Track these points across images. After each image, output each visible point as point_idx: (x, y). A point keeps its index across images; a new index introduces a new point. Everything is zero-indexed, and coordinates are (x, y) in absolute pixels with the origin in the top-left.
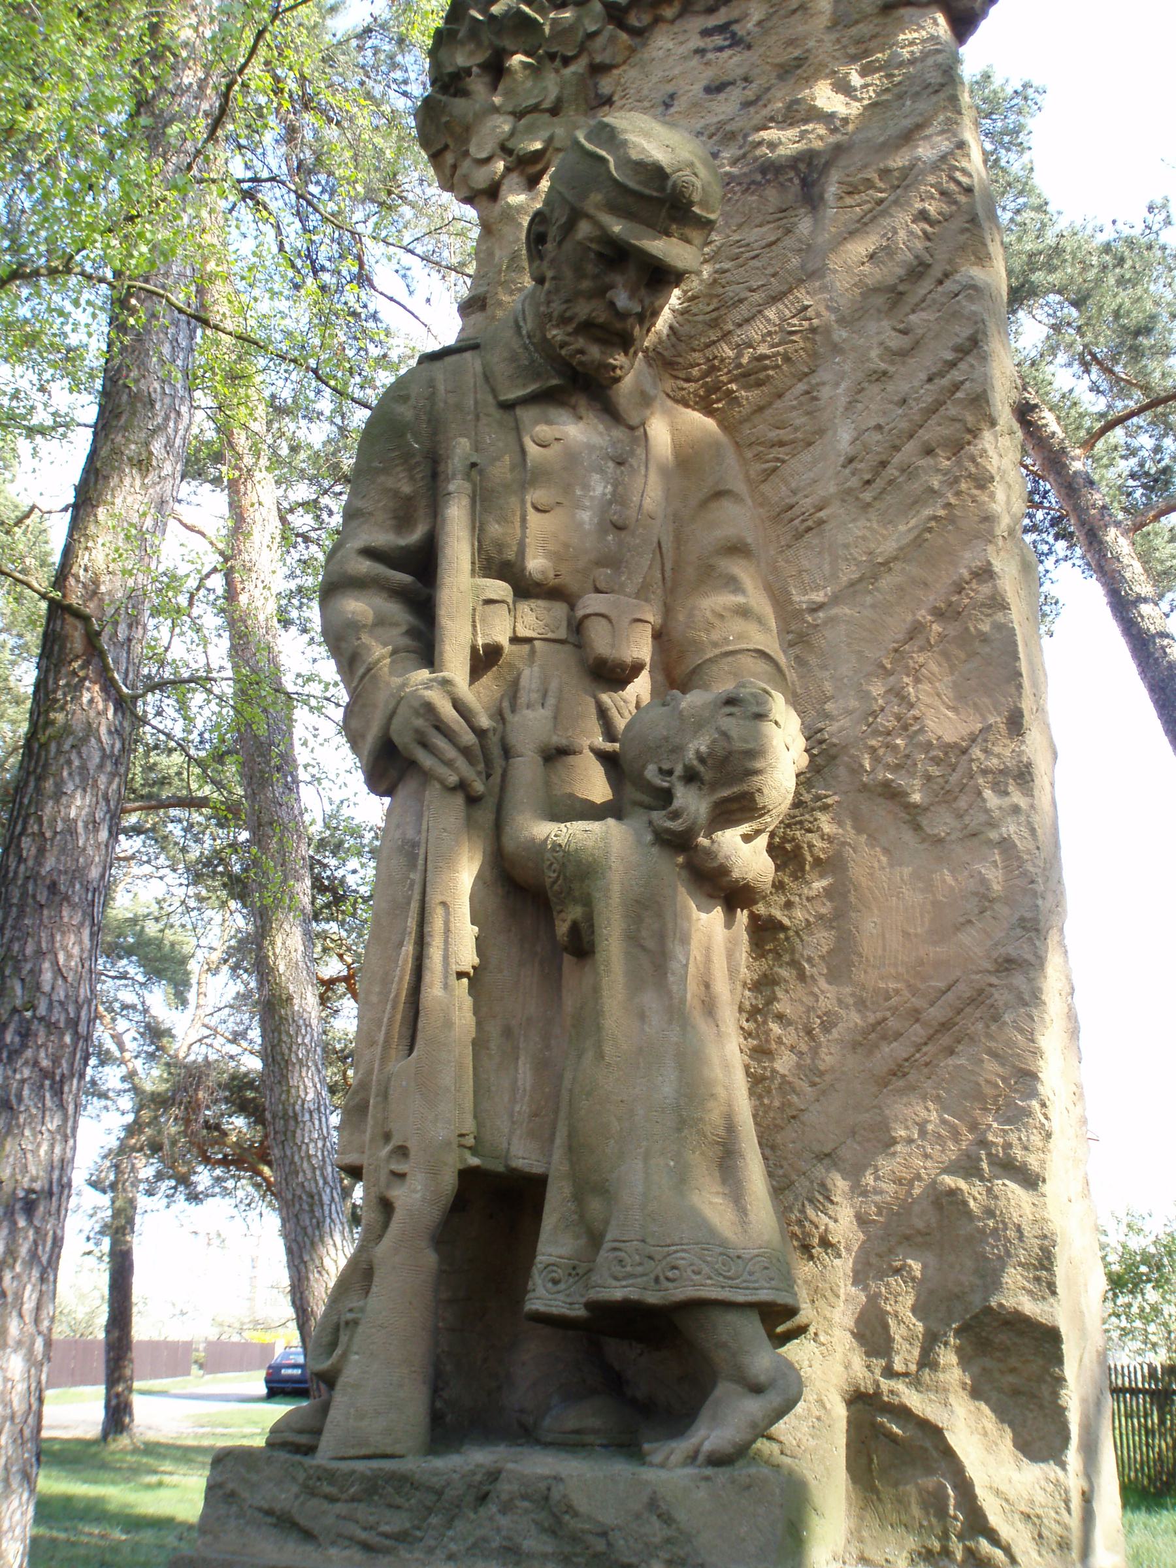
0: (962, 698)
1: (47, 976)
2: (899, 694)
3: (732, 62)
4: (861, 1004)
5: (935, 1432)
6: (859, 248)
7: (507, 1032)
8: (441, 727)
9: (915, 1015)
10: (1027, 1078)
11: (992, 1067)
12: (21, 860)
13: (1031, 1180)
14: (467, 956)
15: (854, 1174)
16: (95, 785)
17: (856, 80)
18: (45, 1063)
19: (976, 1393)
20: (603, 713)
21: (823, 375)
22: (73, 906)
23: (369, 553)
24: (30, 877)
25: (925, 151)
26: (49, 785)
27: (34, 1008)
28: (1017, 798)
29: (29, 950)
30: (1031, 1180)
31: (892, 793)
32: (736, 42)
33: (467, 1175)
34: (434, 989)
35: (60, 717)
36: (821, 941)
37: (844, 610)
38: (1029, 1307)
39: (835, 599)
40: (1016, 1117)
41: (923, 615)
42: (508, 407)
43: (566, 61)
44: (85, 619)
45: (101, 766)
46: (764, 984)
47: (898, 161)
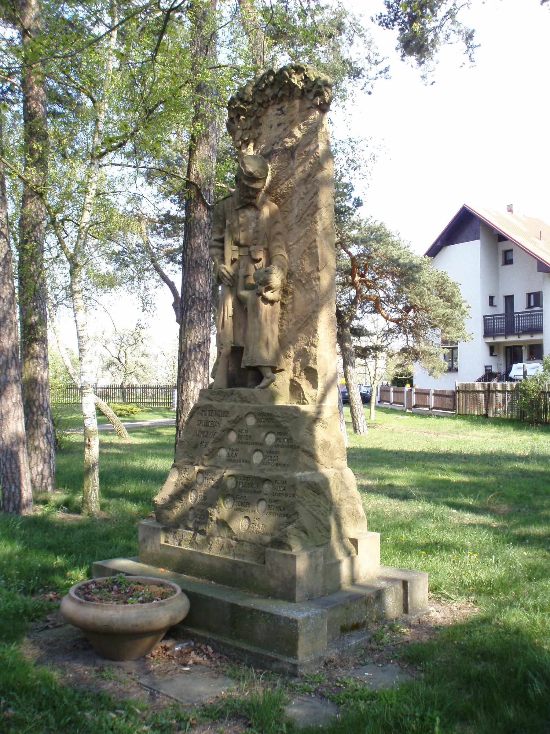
0: (311, 265)
1: (197, 286)
2: (301, 263)
3: (282, 118)
4: (295, 317)
5: (299, 385)
6: (301, 169)
7: (239, 324)
8: (225, 276)
9: (302, 320)
10: (316, 330)
11: (312, 328)
12: (187, 255)
13: (315, 347)
14: (230, 312)
15: (293, 345)
16: (204, 233)
17: (302, 127)
18: (199, 309)
19: (307, 379)
20: (255, 268)
21: (294, 197)
22: (202, 267)
23: (215, 240)
24: (191, 260)
25: (312, 148)
26: (192, 234)
27: (195, 295)
28: (318, 283)
29: (192, 280)
30: (315, 347)
31: (300, 281)
32: (283, 113)
33: (232, 347)
34: (226, 319)
35: (193, 214)
36: (290, 307)
37: (295, 246)
38: (313, 366)
39: (294, 244)
40: (314, 336)
41: (306, 248)
42: (237, 210)
43: (252, 117)
44: (196, 186)
45: (205, 227)
46: (282, 314)
47: (307, 149)
